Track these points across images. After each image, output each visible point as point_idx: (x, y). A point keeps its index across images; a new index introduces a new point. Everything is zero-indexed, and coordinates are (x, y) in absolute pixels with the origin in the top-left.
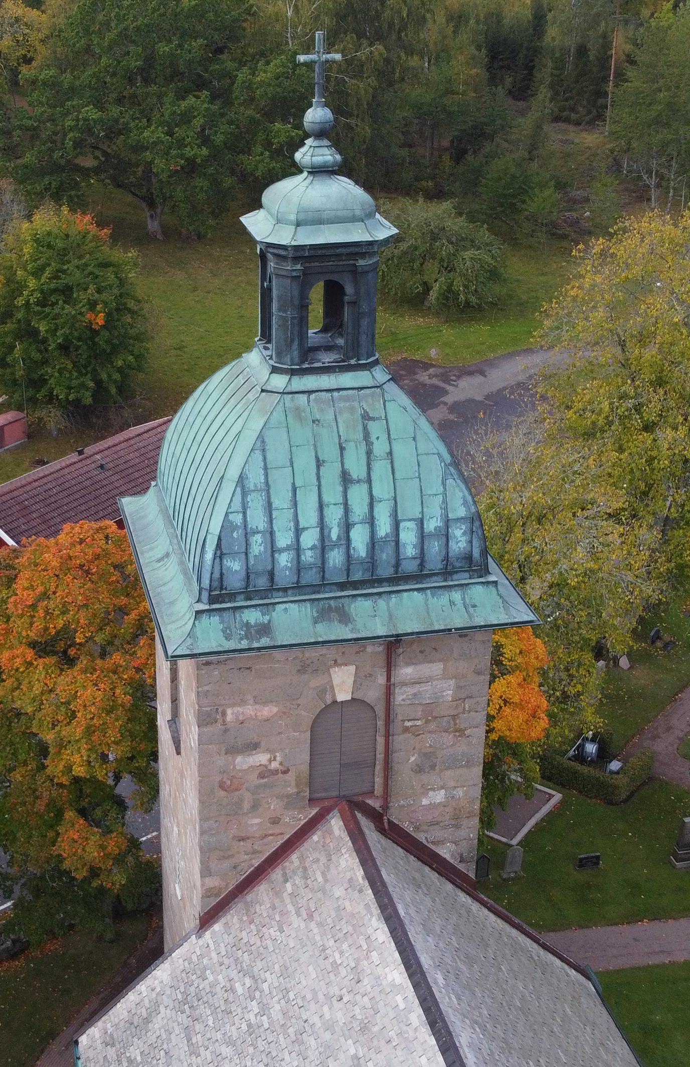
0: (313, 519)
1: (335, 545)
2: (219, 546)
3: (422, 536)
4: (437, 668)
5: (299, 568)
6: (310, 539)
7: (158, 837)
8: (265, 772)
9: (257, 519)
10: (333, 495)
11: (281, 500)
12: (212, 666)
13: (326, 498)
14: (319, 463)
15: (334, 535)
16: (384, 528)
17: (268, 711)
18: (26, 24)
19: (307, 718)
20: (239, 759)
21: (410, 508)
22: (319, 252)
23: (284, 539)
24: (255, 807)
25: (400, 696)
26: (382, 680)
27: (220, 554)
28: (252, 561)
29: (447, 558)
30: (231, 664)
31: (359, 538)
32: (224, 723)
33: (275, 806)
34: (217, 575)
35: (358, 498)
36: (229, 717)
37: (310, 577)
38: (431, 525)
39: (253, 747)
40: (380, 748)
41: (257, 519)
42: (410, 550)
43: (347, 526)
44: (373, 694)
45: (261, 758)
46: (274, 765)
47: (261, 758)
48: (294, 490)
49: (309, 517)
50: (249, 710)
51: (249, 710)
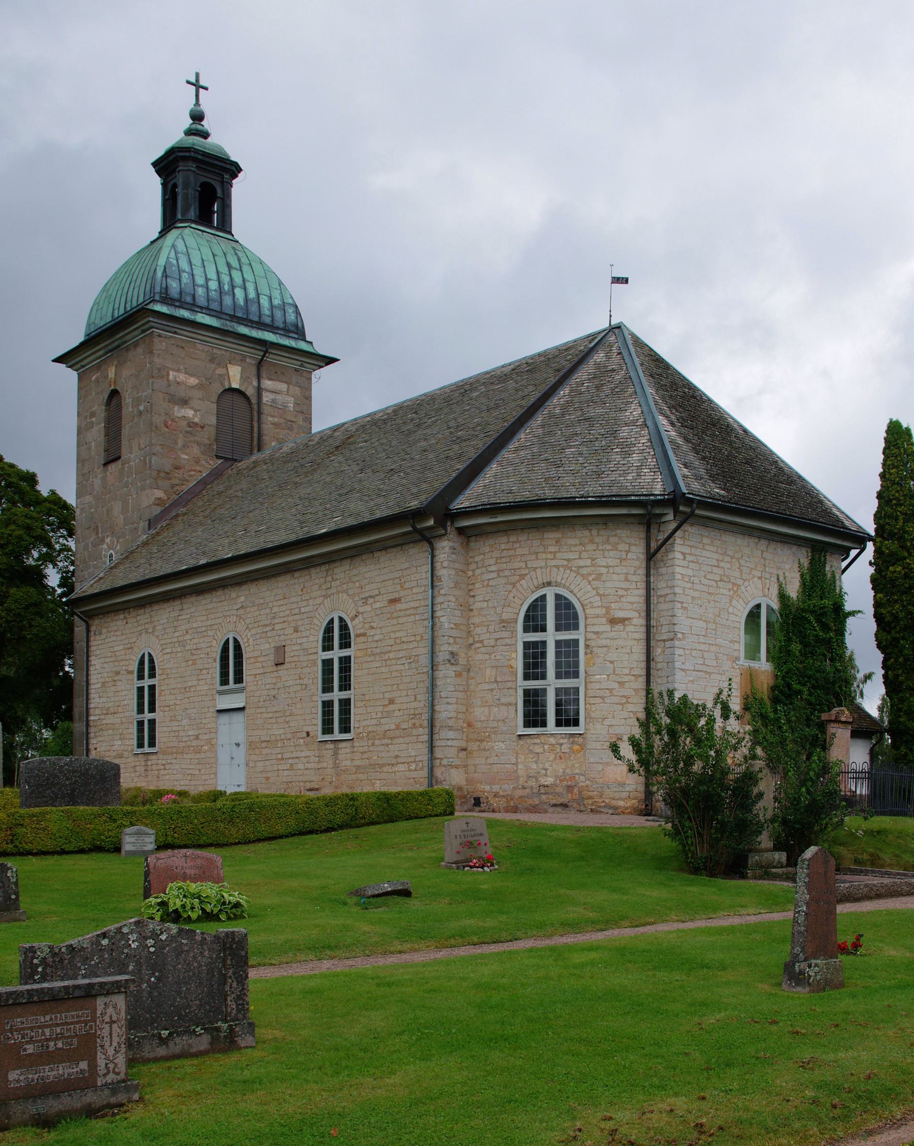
0: (214, 277)
1: (227, 294)
2: (165, 270)
3: (272, 307)
4: (283, 387)
5: (208, 299)
6: (213, 285)
7: (212, 227)
8: (191, 424)
9: (184, 265)
10: (224, 269)
11: (196, 261)
12: (162, 339)
13: (220, 269)
14: (214, 255)
15: (226, 287)
16: (252, 295)
17: (193, 381)
18: (70, 921)
19: (214, 398)
20: (176, 408)
21: (263, 289)
22: (207, 159)
23: (200, 280)
24: (185, 446)
25: (265, 399)
26: (255, 383)
27: (165, 275)
28: (183, 286)
29: (285, 322)
30: (173, 341)
31: (239, 293)
32: (168, 380)
33: (196, 450)
34: (164, 285)
35: (236, 275)
36: (171, 377)
37: (215, 306)
38: (276, 302)
39: (184, 402)
40: (256, 429)
41: (184, 265)
42: (266, 311)
43: (233, 287)
44: (250, 392)
45: (190, 413)
46: (196, 420)
47: (190, 413)
48: (203, 261)
49: (212, 274)
50: (182, 377)
51: (182, 377)
